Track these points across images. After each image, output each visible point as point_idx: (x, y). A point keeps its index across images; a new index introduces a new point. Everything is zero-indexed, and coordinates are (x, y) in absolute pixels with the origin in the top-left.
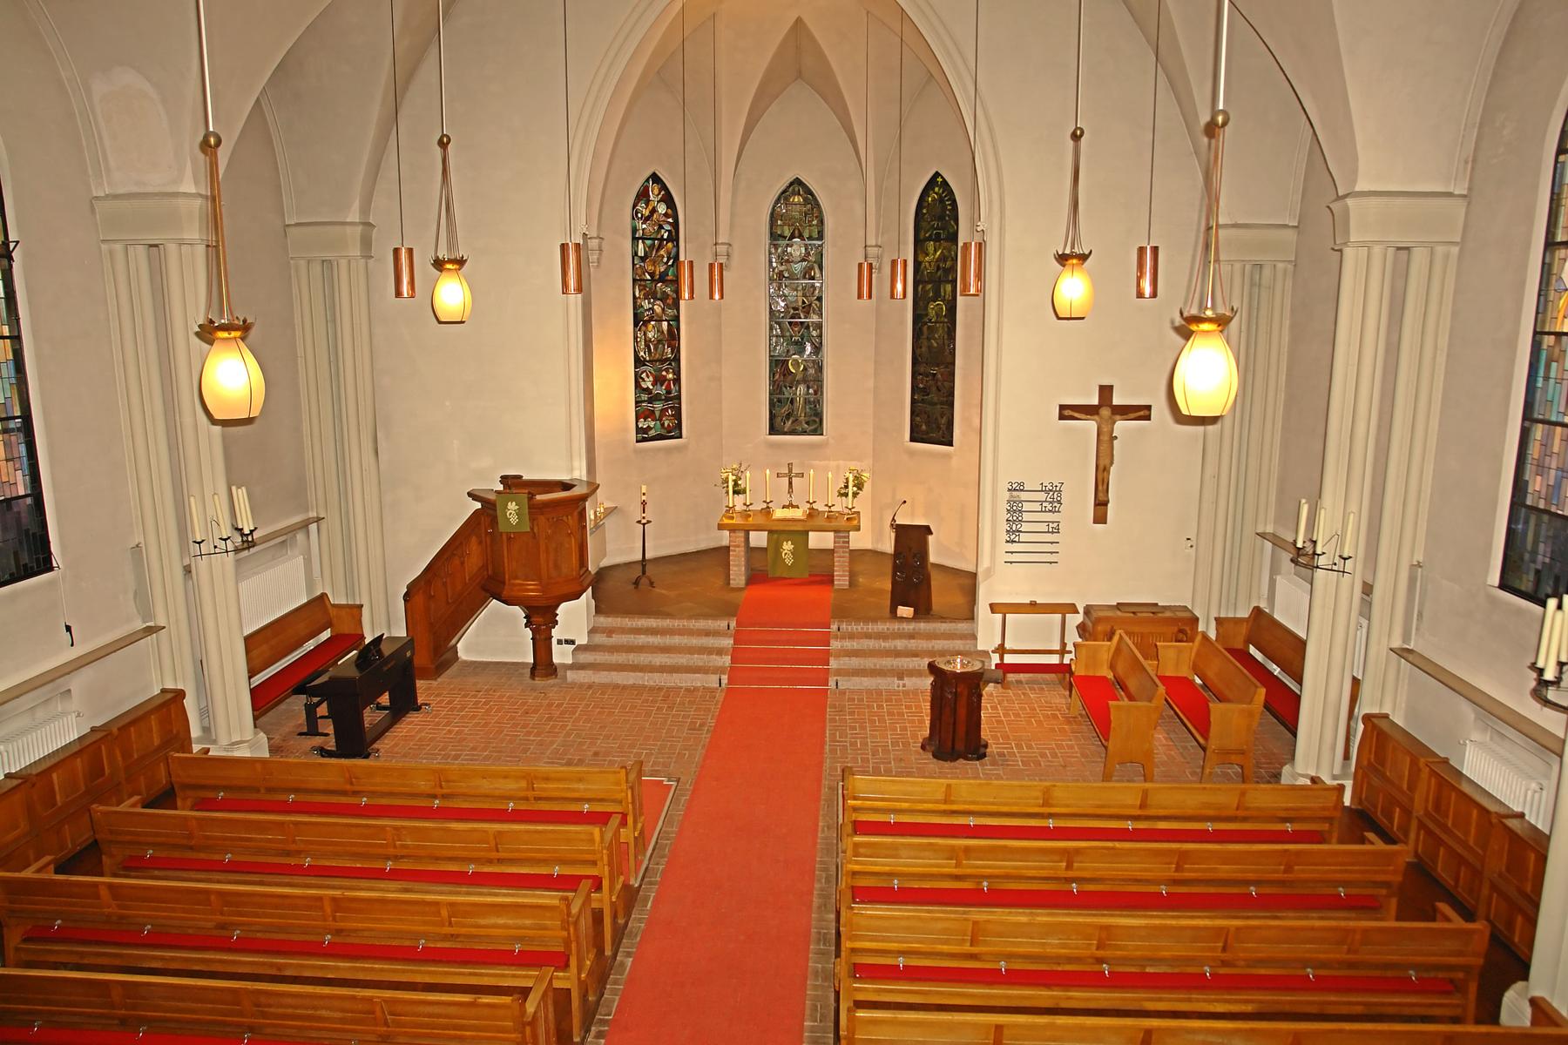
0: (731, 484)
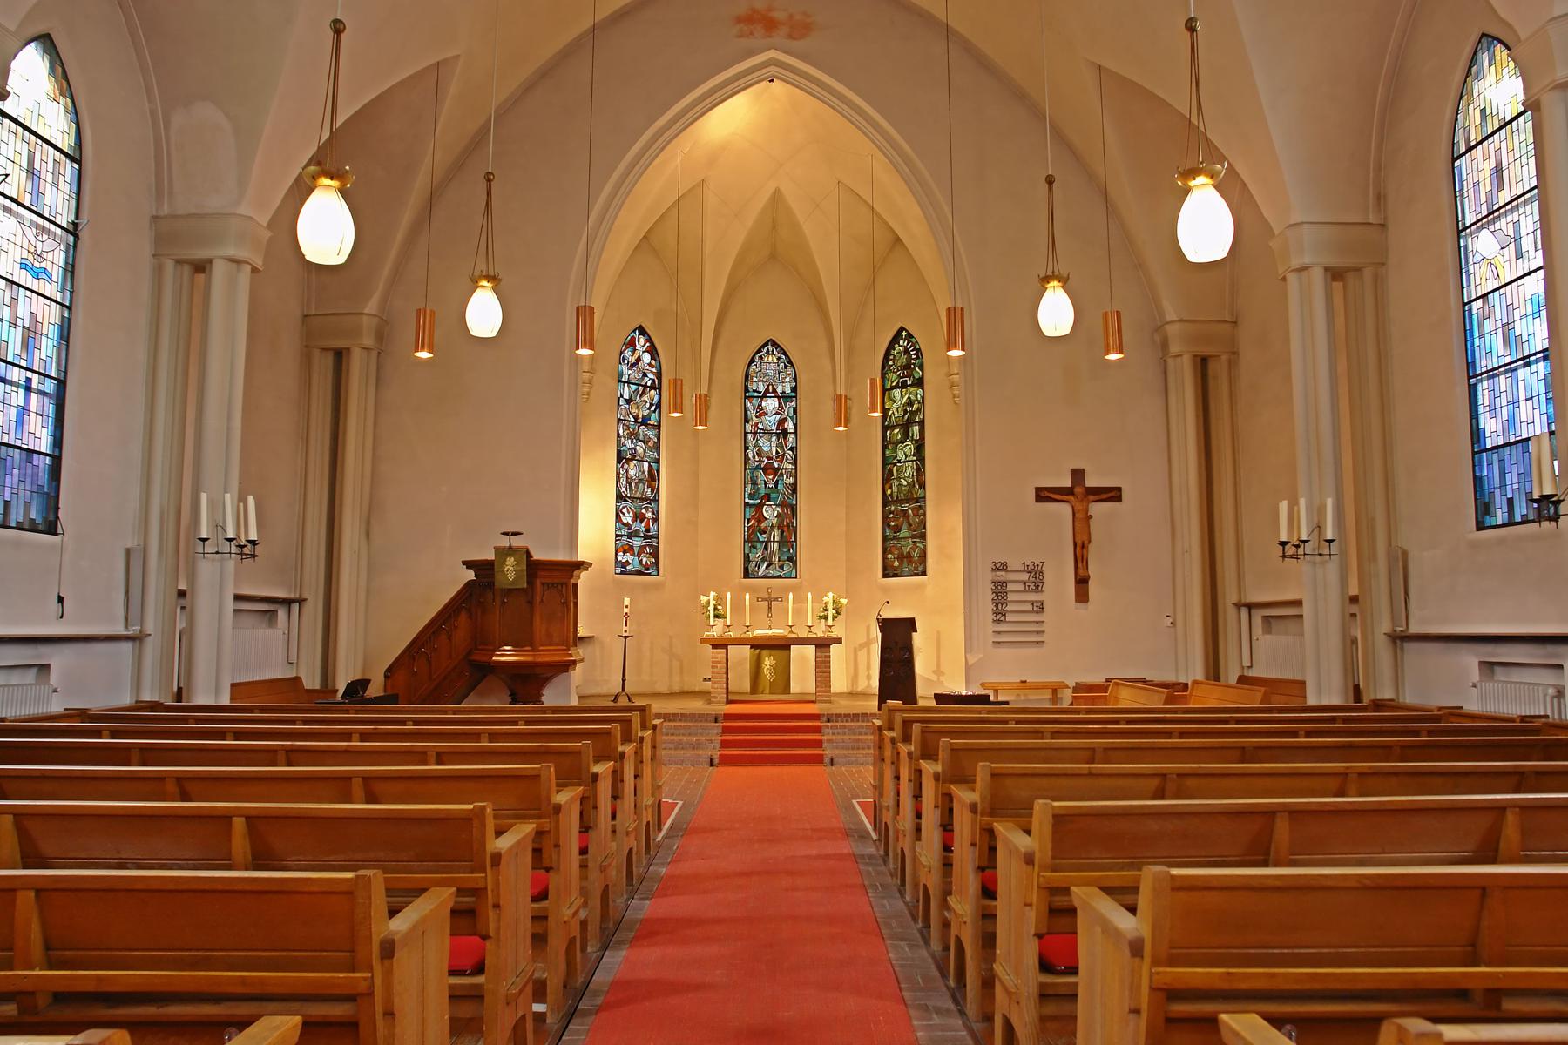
0: (711, 608)
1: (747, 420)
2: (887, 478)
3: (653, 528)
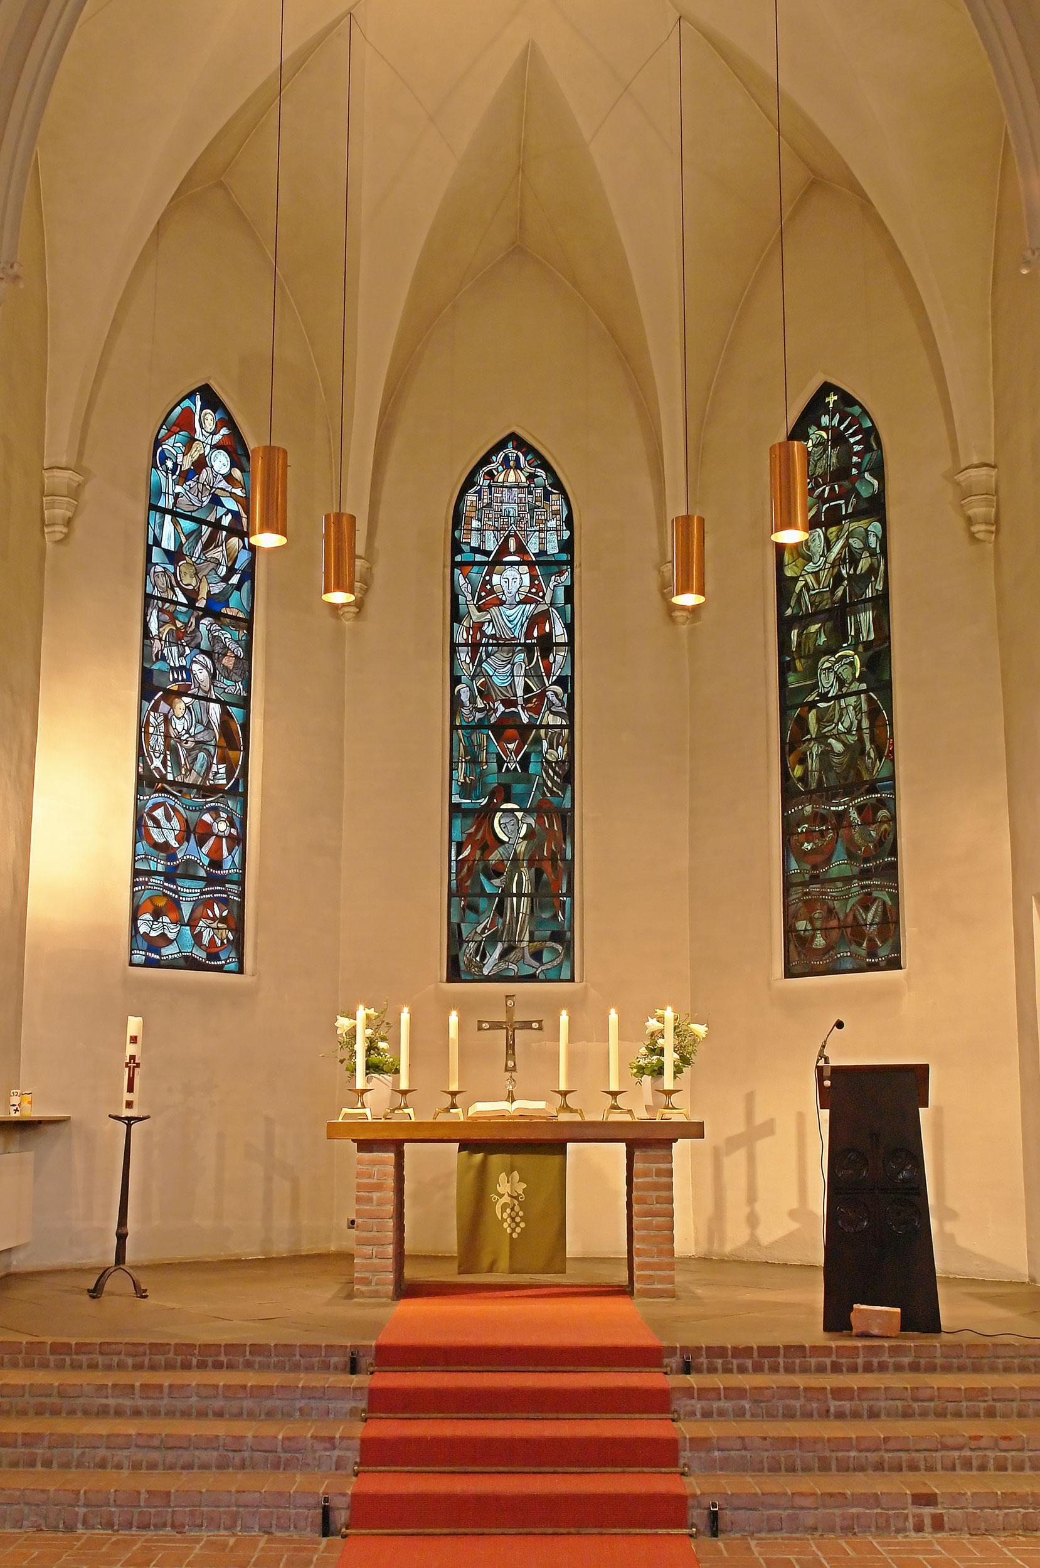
0: (360, 1047)
1: (456, 617)
2: (792, 743)
3: (229, 861)
